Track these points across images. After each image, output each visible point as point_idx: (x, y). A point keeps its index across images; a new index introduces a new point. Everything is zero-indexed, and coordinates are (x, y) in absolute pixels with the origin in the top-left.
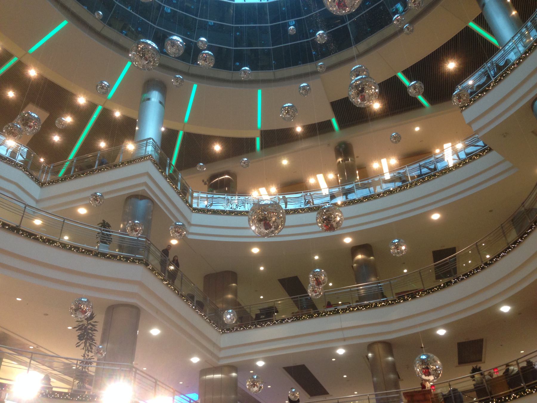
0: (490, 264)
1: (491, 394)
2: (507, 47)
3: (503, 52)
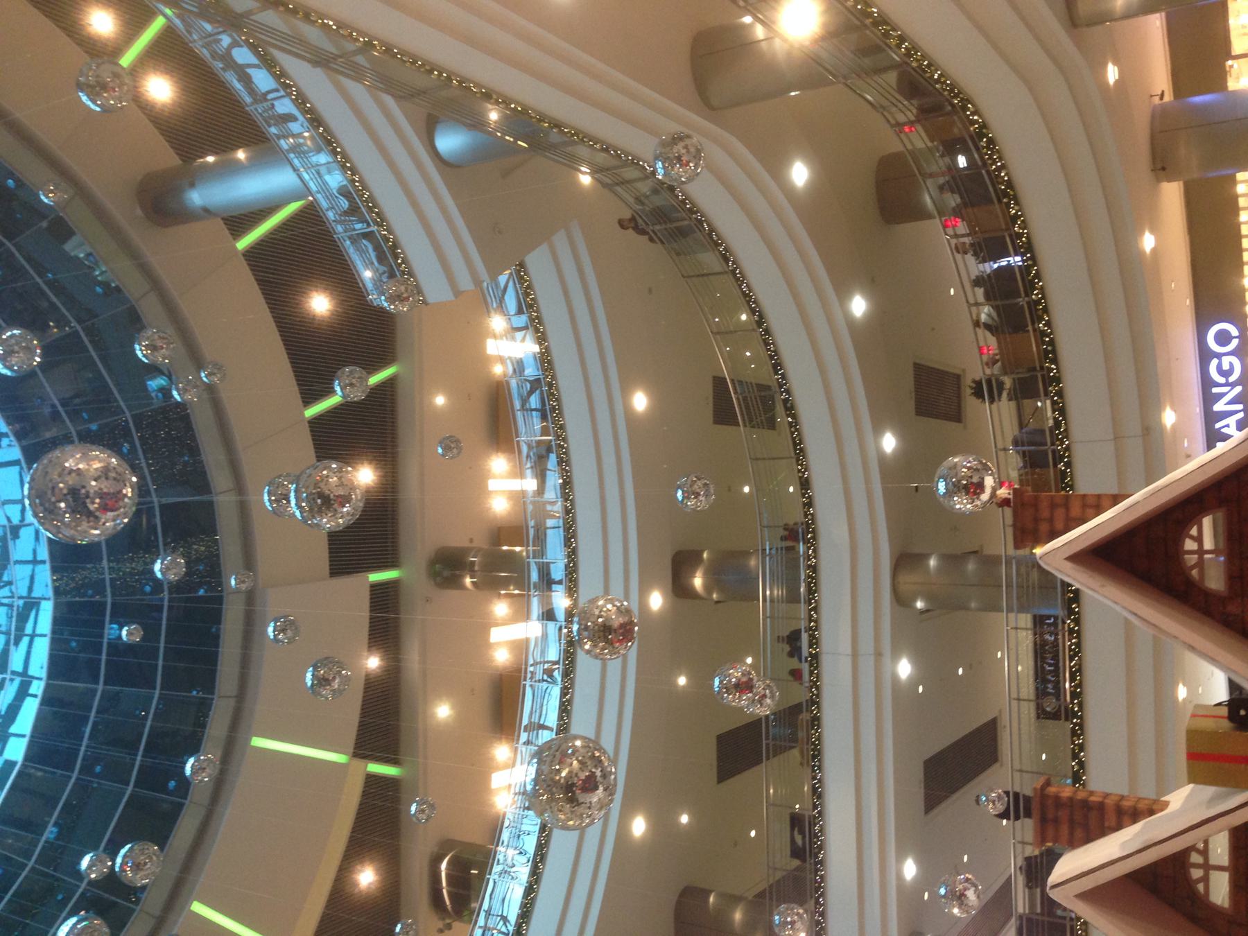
0: (761, 317)
1: (1034, 369)
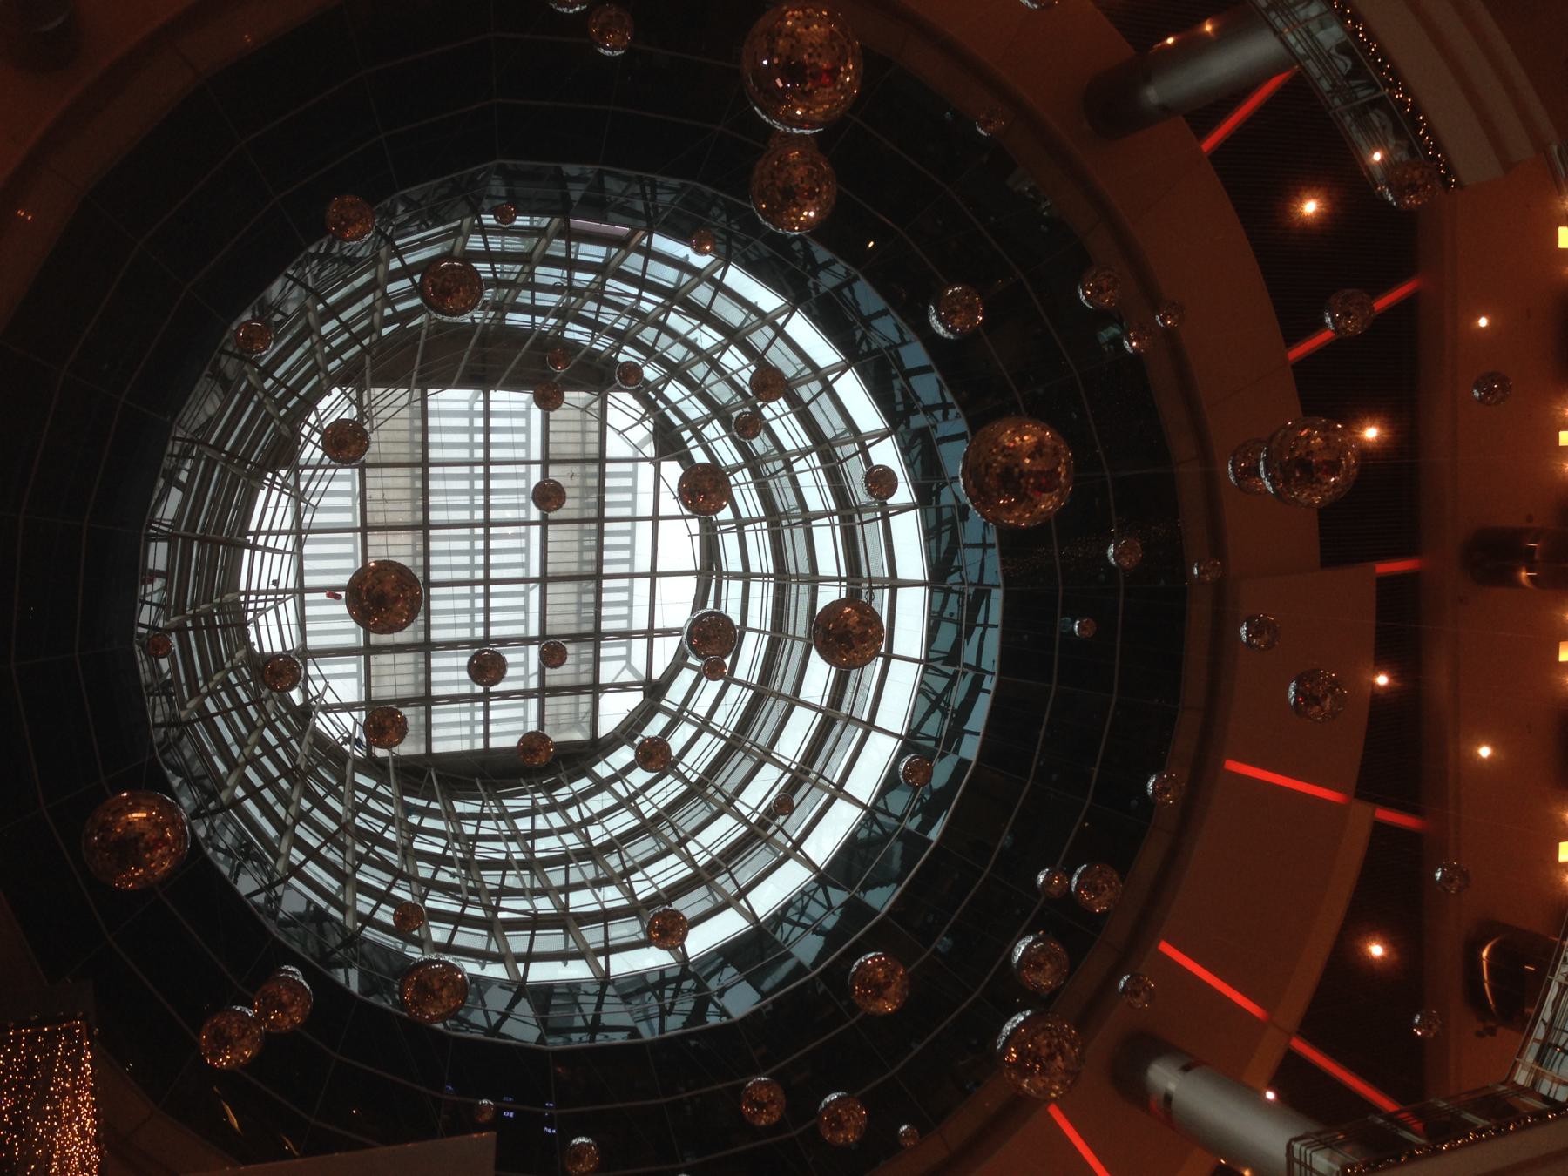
2: (1300, 50)
3: (1309, 62)
